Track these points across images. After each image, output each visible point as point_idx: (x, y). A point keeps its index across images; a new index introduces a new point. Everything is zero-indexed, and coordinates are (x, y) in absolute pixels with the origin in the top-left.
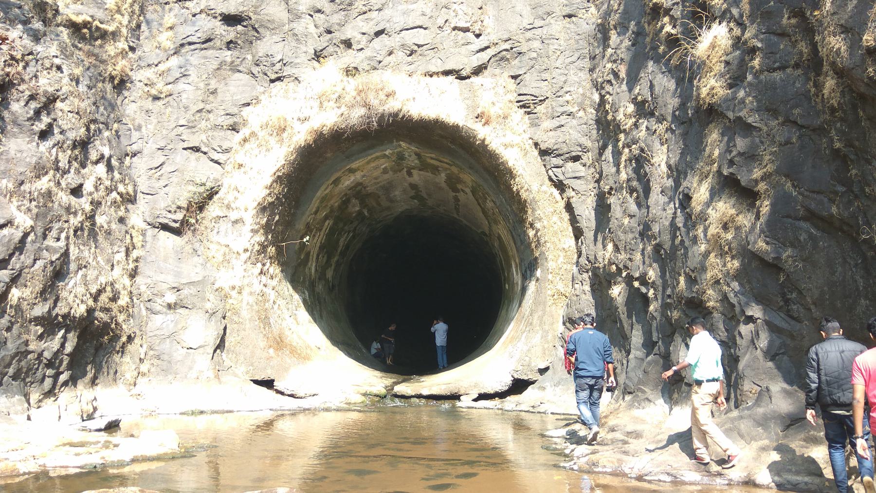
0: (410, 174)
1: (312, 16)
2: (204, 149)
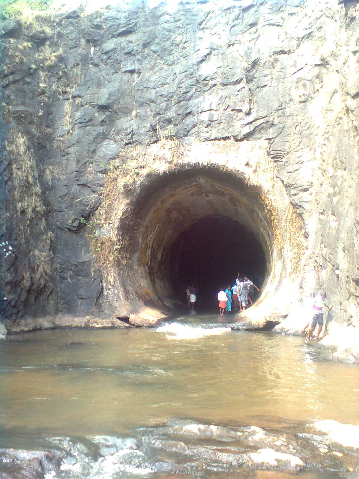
0: (207, 196)
1: (149, 104)
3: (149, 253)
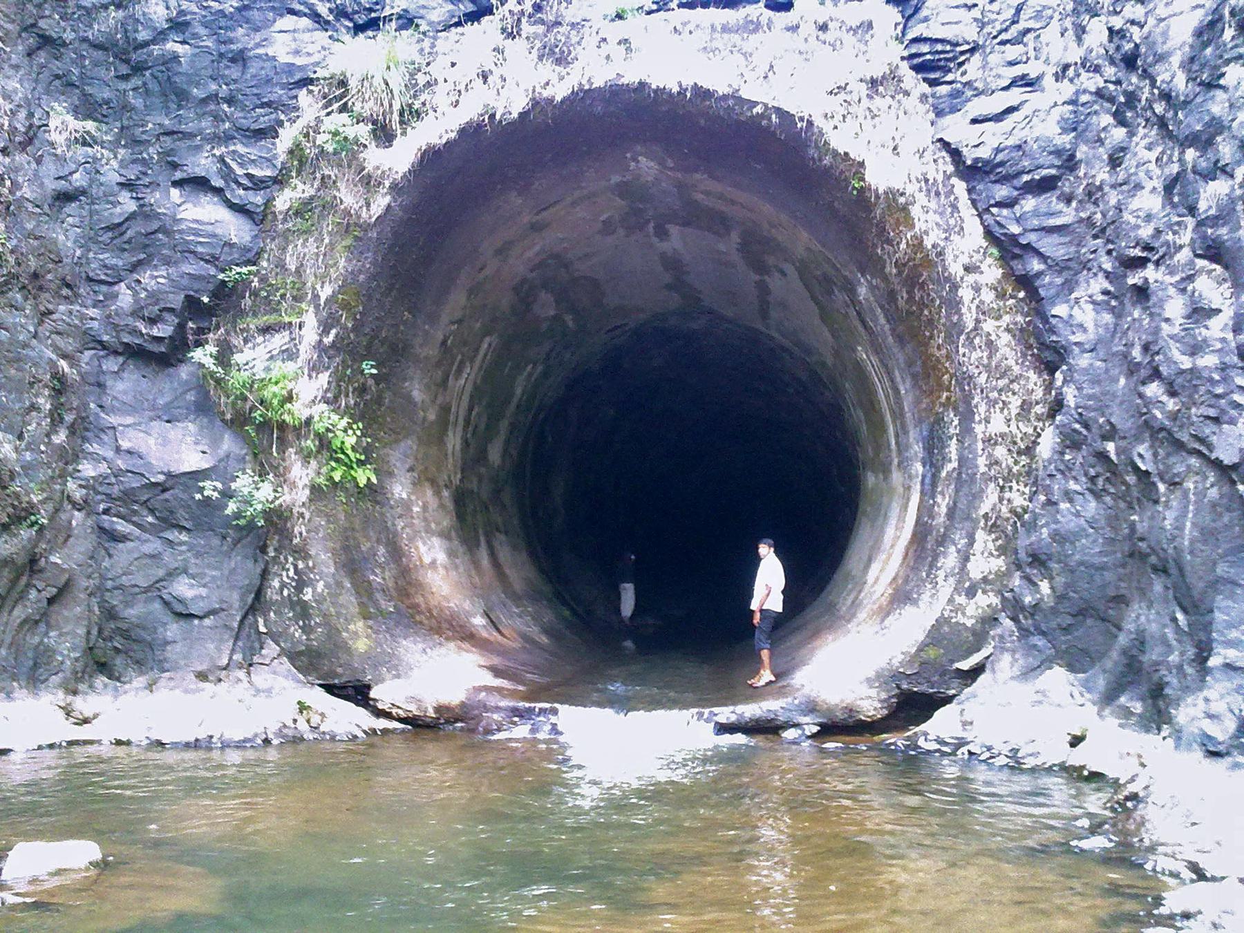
0: (662, 233)
2: (218, 182)
3: (454, 441)
